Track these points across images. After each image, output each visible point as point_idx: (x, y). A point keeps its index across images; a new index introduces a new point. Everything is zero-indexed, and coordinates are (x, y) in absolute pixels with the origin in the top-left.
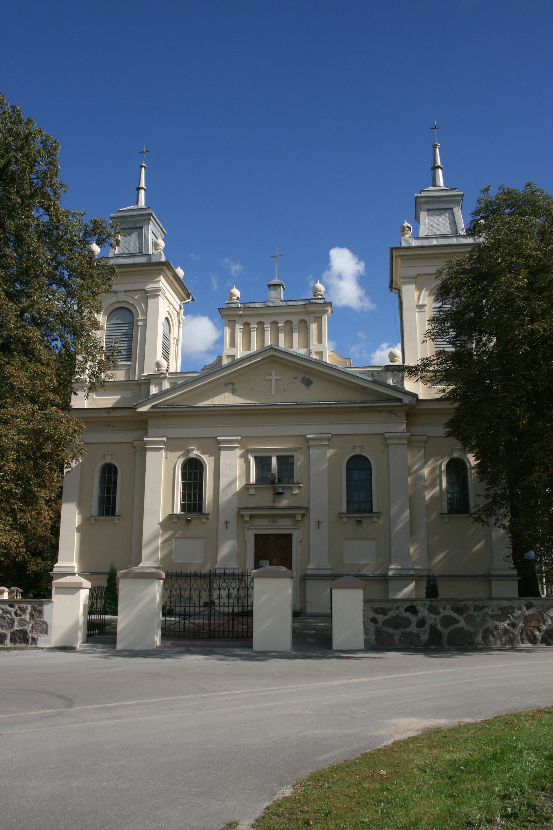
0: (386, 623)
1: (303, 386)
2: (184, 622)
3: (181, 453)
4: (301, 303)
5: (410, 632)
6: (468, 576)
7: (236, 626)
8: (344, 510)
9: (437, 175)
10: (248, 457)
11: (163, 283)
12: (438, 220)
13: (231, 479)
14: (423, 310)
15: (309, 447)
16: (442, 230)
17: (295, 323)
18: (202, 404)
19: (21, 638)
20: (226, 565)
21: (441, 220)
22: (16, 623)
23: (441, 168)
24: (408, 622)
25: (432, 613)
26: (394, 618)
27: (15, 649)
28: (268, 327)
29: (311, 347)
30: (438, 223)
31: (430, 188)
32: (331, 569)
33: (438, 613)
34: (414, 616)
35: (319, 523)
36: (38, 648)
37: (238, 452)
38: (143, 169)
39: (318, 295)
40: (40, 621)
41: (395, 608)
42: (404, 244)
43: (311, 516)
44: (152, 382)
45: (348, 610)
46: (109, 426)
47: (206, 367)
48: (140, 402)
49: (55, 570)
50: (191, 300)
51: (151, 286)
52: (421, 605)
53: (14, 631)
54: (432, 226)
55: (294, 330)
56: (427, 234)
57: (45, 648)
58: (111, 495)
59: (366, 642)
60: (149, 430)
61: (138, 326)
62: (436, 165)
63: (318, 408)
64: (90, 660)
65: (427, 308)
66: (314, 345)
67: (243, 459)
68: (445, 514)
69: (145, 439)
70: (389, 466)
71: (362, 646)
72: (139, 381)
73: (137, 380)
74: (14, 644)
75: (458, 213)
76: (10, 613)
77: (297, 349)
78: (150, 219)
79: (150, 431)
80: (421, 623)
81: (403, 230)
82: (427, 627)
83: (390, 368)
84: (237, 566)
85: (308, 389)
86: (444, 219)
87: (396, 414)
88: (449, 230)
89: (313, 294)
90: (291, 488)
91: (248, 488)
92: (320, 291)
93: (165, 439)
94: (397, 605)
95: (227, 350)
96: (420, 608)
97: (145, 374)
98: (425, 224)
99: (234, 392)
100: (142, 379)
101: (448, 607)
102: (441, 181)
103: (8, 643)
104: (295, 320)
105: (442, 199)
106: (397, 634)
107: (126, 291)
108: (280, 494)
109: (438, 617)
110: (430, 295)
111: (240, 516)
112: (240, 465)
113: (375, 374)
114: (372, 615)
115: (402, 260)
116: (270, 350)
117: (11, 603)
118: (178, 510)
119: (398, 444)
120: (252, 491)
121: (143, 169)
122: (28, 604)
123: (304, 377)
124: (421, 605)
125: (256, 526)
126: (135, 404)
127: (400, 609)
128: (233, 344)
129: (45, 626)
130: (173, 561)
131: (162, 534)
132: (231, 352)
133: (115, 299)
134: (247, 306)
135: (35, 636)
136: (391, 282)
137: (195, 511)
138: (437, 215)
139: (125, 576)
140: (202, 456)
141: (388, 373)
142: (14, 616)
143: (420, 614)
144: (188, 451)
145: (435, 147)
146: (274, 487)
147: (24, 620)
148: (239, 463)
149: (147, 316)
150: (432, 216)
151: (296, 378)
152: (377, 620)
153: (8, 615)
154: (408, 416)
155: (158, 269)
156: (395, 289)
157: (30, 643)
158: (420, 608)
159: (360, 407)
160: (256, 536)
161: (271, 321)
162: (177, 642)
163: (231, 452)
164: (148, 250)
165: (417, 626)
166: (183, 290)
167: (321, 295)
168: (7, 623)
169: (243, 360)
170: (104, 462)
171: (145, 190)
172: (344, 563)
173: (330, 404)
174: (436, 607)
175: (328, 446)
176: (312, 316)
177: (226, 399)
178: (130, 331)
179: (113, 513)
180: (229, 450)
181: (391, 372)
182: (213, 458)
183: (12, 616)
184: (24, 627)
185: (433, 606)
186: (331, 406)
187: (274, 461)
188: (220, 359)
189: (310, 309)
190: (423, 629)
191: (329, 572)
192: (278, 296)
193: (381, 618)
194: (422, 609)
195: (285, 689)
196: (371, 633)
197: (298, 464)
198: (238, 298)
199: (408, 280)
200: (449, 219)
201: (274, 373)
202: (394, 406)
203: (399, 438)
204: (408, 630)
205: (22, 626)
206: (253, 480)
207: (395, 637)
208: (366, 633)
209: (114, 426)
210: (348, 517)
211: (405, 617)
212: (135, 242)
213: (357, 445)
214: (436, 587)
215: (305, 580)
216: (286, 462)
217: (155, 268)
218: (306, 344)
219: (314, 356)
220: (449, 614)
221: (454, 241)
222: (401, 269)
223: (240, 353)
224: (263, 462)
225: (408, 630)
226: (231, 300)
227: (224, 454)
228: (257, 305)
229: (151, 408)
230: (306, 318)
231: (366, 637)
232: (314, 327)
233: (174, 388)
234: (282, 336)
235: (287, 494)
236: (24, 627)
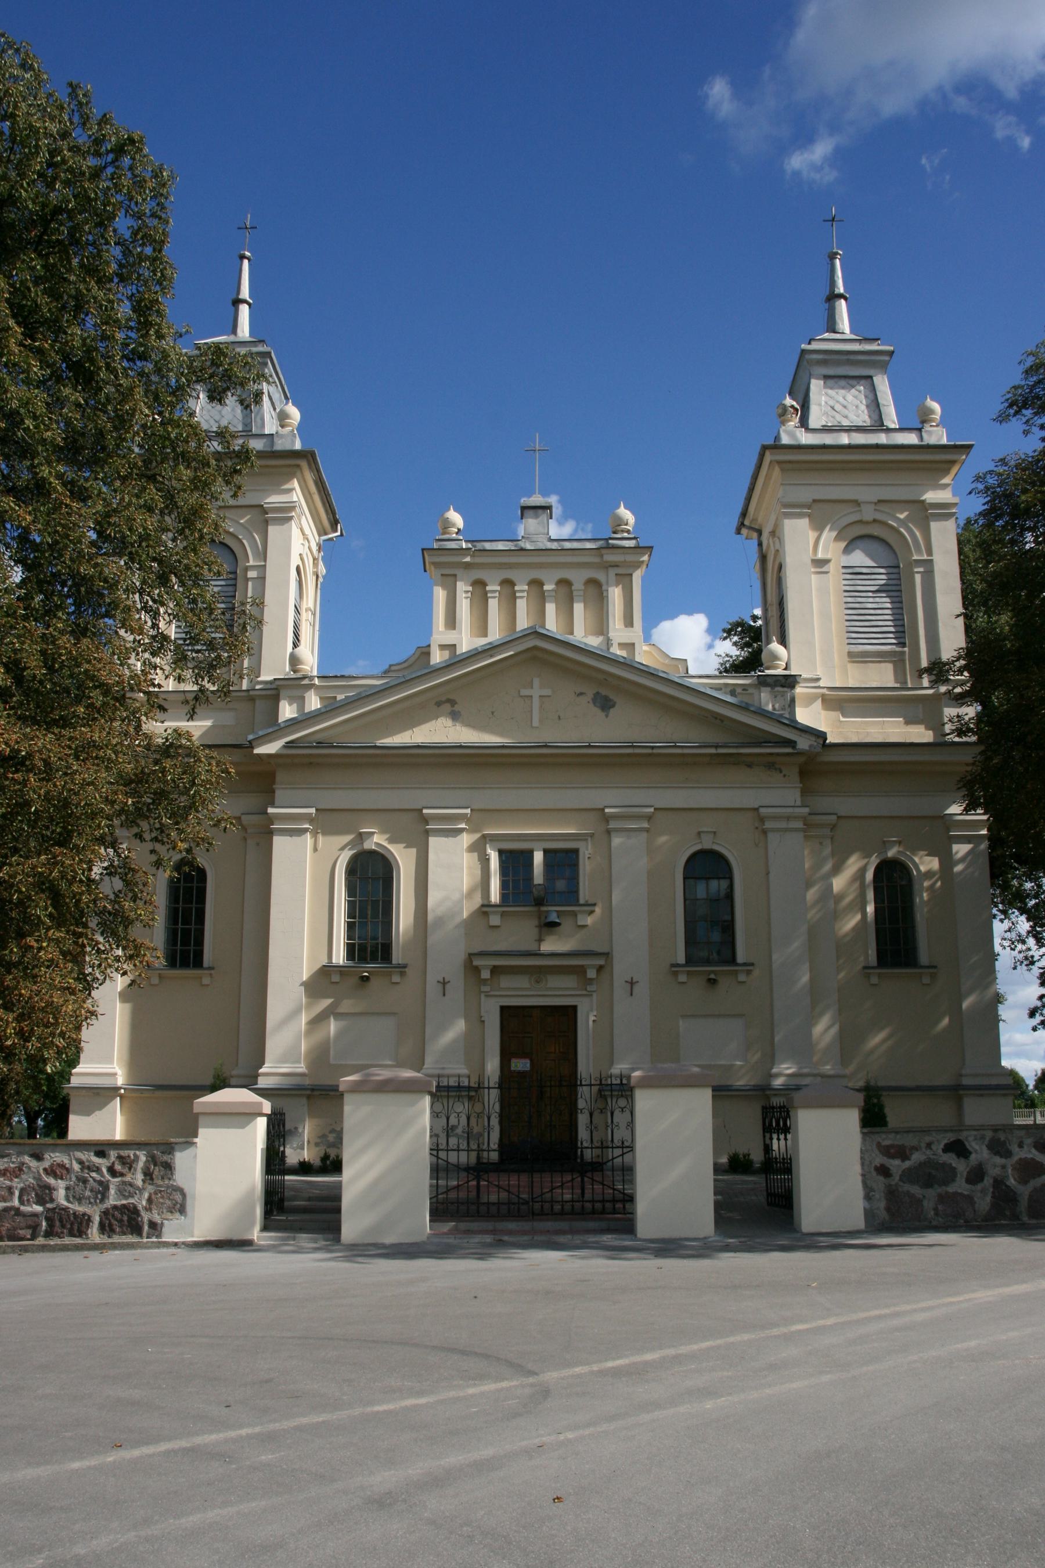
0: (909, 1176)
2: (478, 1183)
3: (348, 838)
4: (588, 545)
5: (956, 1194)
6: (918, 1088)
7: (588, 1186)
8: (681, 959)
9: (837, 311)
11: (295, 493)
12: (844, 398)
14: (824, 569)
15: (608, 832)
16: (852, 417)
17: (578, 585)
18: (381, 742)
19: (126, 1222)
20: (443, 1068)
21: (850, 398)
22: (112, 1191)
23: (846, 299)
24: (950, 1175)
25: (997, 1153)
26: (922, 1165)
27: (115, 1246)
28: (523, 591)
29: (611, 634)
30: (845, 403)
31: (826, 335)
33: (1008, 1154)
34: (962, 1160)
35: (632, 983)
36: (166, 1244)
37: (466, 839)
38: (246, 262)
39: (623, 531)
40: (168, 1187)
41: (923, 1145)
42: (785, 440)
44: (282, 693)
45: (829, 1150)
47: (393, 668)
48: (261, 733)
49: (75, 1081)
50: (339, 533)
51: (274, 499)
52: (975, 1139)
53: (107, 1209)
54: (833, 408)
55: (575, 598)
56: (824, 423)
57: (184, 1243)
58: (193, 927)
59: (869, 1214)
61: (247, 580)
62: (837, 291)
63: (629, 755)
64: (297, 1265)
65: (831, 567)
66: (618, 631)
67: (476, 854)
68: (873, 968)
69: (270, 810)
70: (768, 874)
71: (861, 1225)
72: (251, 693)
73: (248, 691)
74: (109, 1237)
75: (882, 384)
76: (98, 1170)
77: (582, 634)
78: (266, 364)
79: (279, 795)
80: (976, 1175)
81: (783, 413)
82: (988, 1181)
83: (769, 680)
84: (465, 1071)
85: (607, 716)
86: (855, 397)
87: (781, 772)
88: (867, 418)
89: (610, 531)
90: (575, 914)
91: (486, 914)
92: (626, 524)
93: (313, 811)
94: (928, 1139)
95: (440, 634)
96: (973, 1144)
97: (266, 677)
98: (820, 405)
99: (455, 716)
100: (258, 687)
101: (1029, 1141)
102: (844, 323)
103: (94, 1234)
104: (578, 578)
105: (852, 357)
106: (929, 1198)
108: (553, 925)
109: (1010, 1163)
110: (837, 539)
111: (471, 968)
112: (470, 868)
113: (739, 690)
114: (879, 1160)
115: (782, 470)
116: (532, 637)
117: (101, 1148)
118: (340, 957)
119: (786, 830)
120: (495, 920)
121: (246, 262)
122: (139, 1149)
123: (598, 693)
124: (975, 1139)
125: (551, 989)
126: (251, 737)
127: (934, 1147)
128: (452, 622)
129: (178, 1197)
130: (332, 1062)
132: (449, 638)
134: (479, 546)
135: (157, 1218)
136: (744, 514)
137: (374, 959)
138: (843, 388)
139: (357, 1088)
141: (763, 689)
142: (108, 1177)
143: (973, 1156)
144: (361, 837)
145: (832, 256)
146: (540, 912)
147: (131, 1185)
149: (265, 561)
150: (831, 388)
151: (581, 694)
152: (889, 1169)
153: (94, 1174)
154: (805, 773)
155: (289, 466)
156: (750, 528)
157: (145, 1234)
158: (973, 1145)
159: (711, 755)
160: (503, 1009)
161: (529, 579)
162: (463, 1226)
164: (263, 426)
165: (969, 1181)
166: (327, 514)
167: (628, 532)
168: (91, 1191)
169: (475, 655)
171: (249, 304)
173: (653, 748)
174: (1004, 1142)
176: (612, 572)
177: (440, 732)
178: (231, 589)
179: (197, 961)
180: (447, 836)
181: (769, 689)
182: (414, 850)
183: (103, 1176)
184: (131, 1201)
185: (999, 1139)
186: (655, 751)
187: (538, 857)
188: (425, 653)
189: (610, 557)
190: (979, 1187)
192: (541, 530)
193: (896, 1165)
194: (977, 1147)
195: (896, 1315)
196: (877, 1196)
197: (586, 867)
198: (459, 530)
199: (793, 509)
200: (866, 397)
201: (536, 682)
202: (778, 754)
203: (788, 818)
204: (951, 1189)
205: (126, 1198)
206: (495, 896)
207: (925, 1203)
208: (868, 1197)
210: (689, 973)
211: (944, 1164)
212: (233, 410)
213: (705, 829)
214: (881, 1107)
216: (564, 861)
217: (284, 462)
218: (601, 627)
219: (616, 651)
220: (1030, 1156)
221: (882, 439)
222: (775, 487)
223: (466, 641)
224: (515, 862)
225: (951, 1189)
226: (444, 533)
227: (435, 843)
228: (500, 546)
229: (284, 747)
230: (600, 576)
231: (868, 1206)
232: (615, 594)
233: (331, 708)
234: (551, 608)
235: (567, 925)
236: (131, 1201)
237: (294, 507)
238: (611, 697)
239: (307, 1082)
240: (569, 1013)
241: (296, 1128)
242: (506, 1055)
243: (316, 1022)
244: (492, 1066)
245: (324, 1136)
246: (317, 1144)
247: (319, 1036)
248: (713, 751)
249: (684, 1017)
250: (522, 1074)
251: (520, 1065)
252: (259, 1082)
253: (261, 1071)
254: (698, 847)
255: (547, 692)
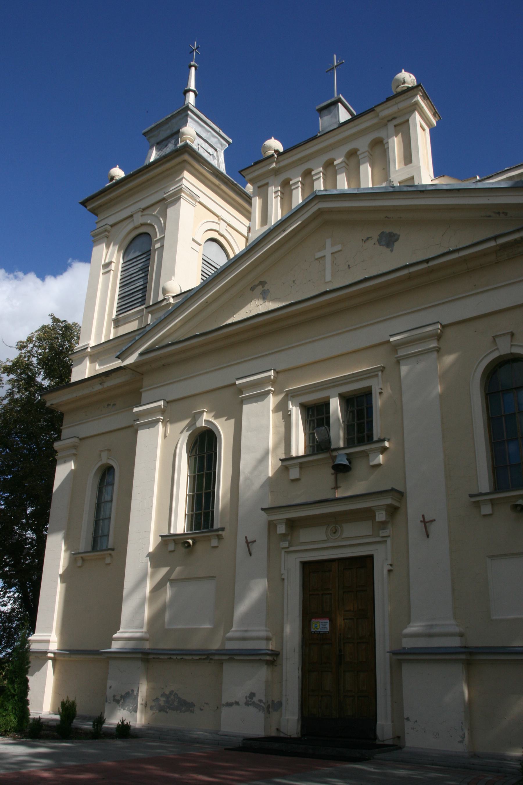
1: (384, 249)
8: (484, 484)
10: (287, 406)
13: (258, 455)
15: (398, 362)
20: (246, 631)
32: (461, 635)
35: (425, 523)
37: (272, 401)
38: (193, 69)
43: (409, 511)
46: (108, 405)
60: (144, 395)
67: (281, 413)
78: (187, 115)
85: (392, 251)
90: (365, 455)
92: (404, 82)
99: (265, 296)
104: (362, 144)
107: (144, 210)
112: (275, 427)
120: (294, 473)
121: (193, 69)
123: (383, 233)
131: (153, 575)
133: (131, 226)
140: (215, 422)
148: (273, 420)
160: (305, 565)
163: (260, 403)
170: (100, 464)
171: (194, 91)
172: (494, 618)
175: (438, 350)
176: (391, 127)
187: (335, 404)
191: (455, 642)
201: (328, 242)
209: (114, 405)
215: (400, 662)
216: (359, 405)
224: (316, 415)
232: (396, 143)
235: (360, 468)
237: (181, 189)
238: (394, 232)
239: (147, 646)
240: (366, 562)
241: (133, 691)
242: (307, 615)
243: (157, 589)
244: (292, 630)
245: (157, 699)
246: (152, 708)
247: (159, 603)
248: (492, 244)
249: (492, 557)
250: (322, 636)
251: (321, 626)
252: (112, 647)
253: (115, 636)
254: (495, 355)
255: (338, 248)
